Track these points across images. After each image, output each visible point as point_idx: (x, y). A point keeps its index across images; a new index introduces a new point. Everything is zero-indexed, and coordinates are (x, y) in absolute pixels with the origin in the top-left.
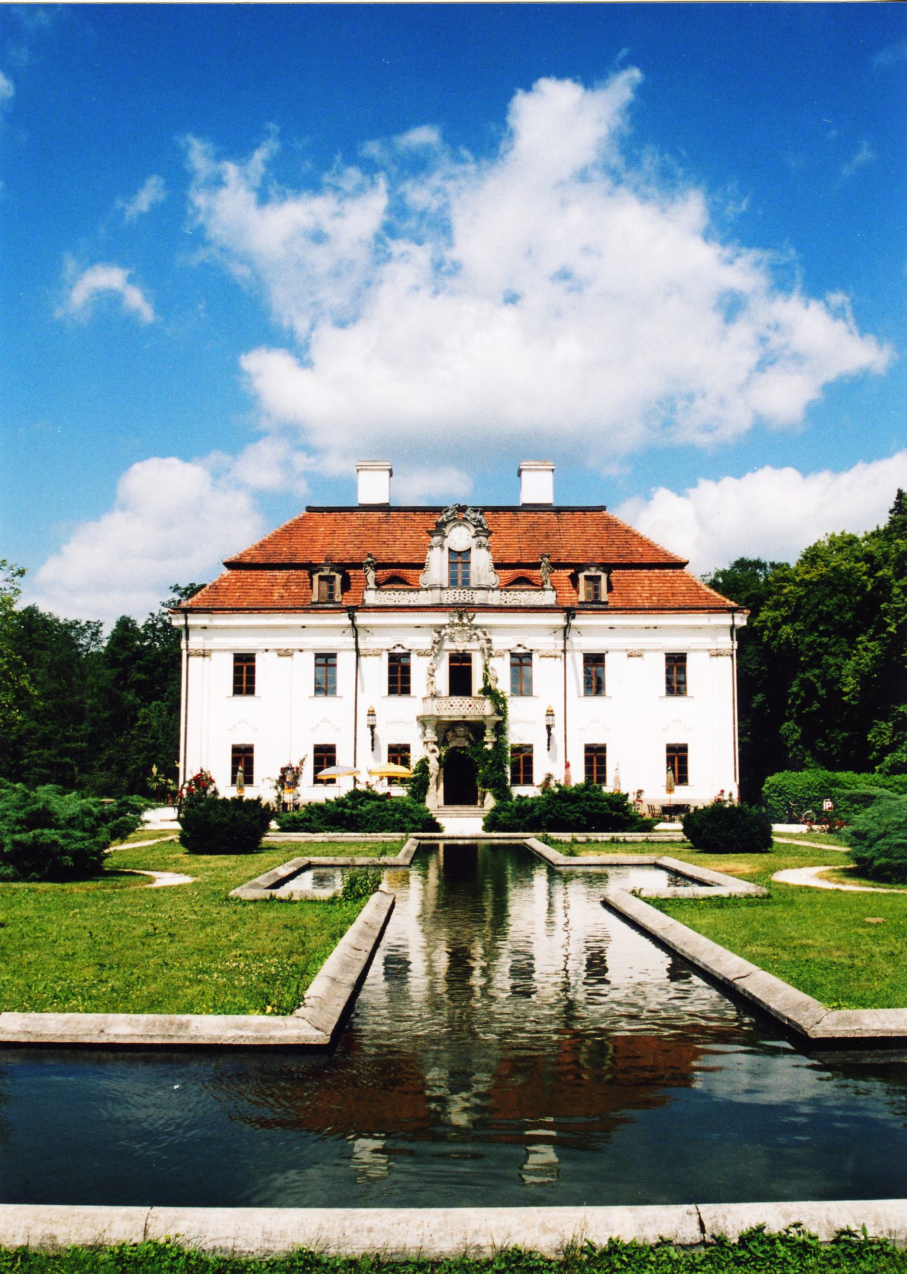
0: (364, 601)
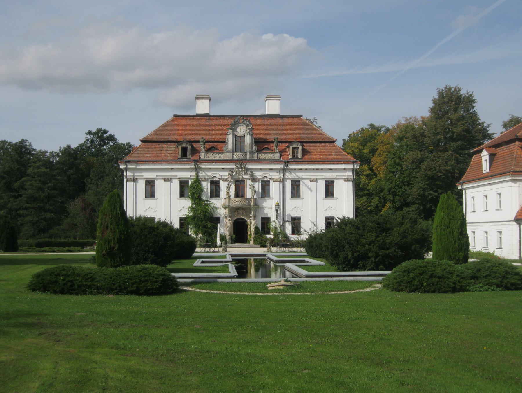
0: (200, 157)
